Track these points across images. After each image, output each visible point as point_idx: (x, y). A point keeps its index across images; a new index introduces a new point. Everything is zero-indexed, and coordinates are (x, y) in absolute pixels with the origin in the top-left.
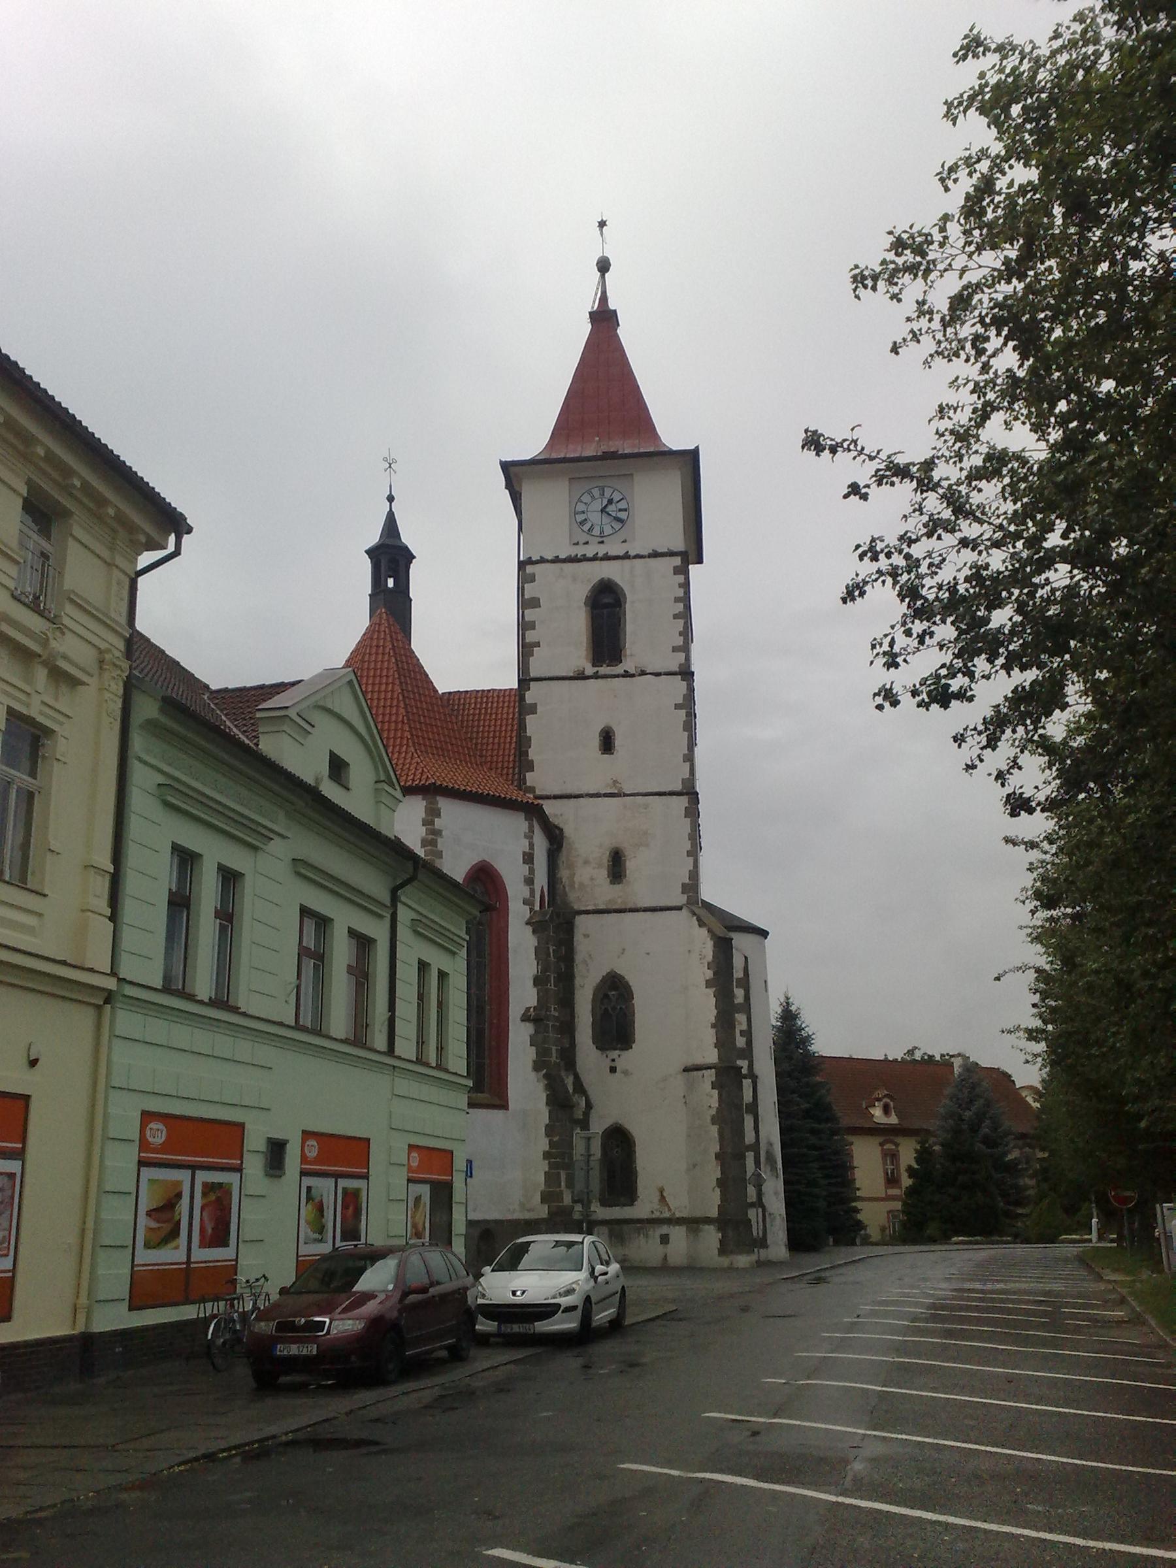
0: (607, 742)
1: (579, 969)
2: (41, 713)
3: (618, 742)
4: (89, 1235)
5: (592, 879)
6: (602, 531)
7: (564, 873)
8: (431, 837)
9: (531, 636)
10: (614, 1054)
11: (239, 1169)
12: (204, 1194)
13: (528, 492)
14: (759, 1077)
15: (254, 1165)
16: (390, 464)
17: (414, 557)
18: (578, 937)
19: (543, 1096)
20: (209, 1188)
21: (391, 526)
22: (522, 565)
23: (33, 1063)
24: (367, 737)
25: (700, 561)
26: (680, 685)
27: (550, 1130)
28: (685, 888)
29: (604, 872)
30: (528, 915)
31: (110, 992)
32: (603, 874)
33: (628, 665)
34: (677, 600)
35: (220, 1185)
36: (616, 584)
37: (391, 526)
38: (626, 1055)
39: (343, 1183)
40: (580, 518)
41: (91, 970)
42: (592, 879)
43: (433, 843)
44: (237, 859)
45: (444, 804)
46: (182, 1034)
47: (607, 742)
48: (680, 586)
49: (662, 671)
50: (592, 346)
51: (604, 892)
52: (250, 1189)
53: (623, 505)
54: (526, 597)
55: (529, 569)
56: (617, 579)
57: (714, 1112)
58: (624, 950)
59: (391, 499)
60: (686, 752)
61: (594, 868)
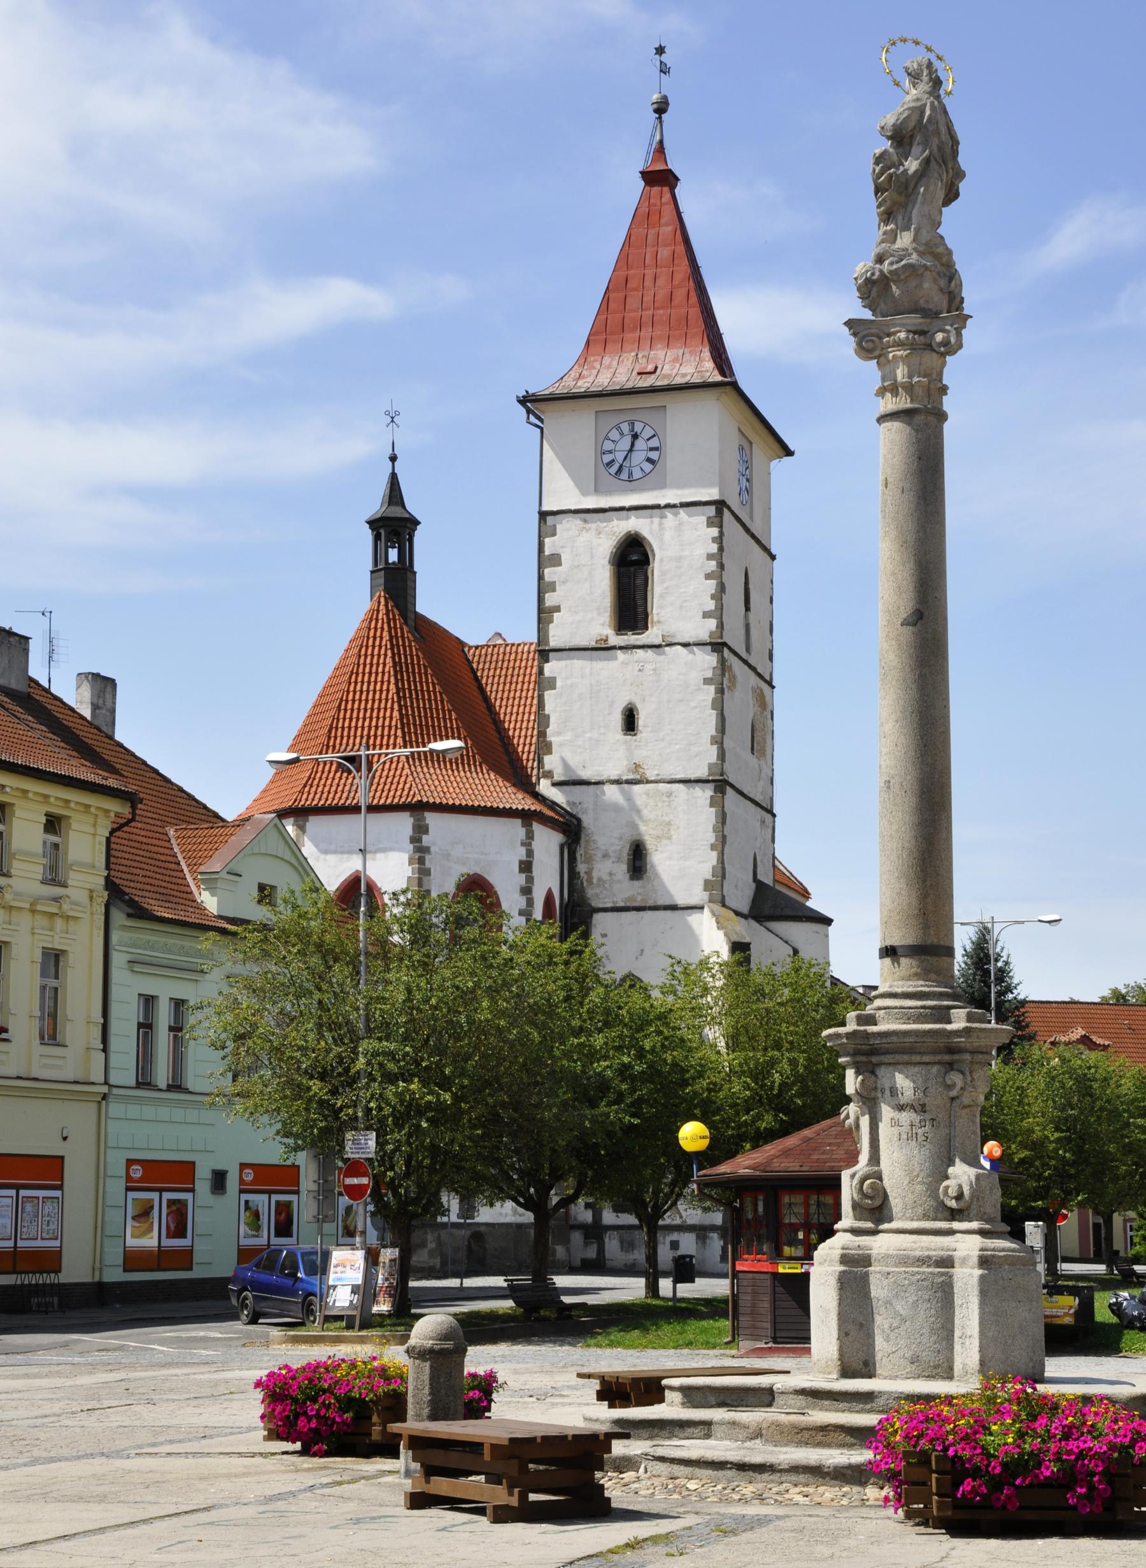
0: (630, 722)
2: (60, 943)
3: (641, 721)
4: (99, 1229)
5: (611, 874)
6: (630, 474)
7: (581, 868)
11: (192, 1190)
12: (168, 1207)
15: (203, 1185)
16: (392, 418)
17: (418, 523)
20: (171, 1202)
21: (395, 494)
22: (543, 515)
23: (65, 1139)
24: (296, 863)
29: (624, 867)
31: (105, 1094)
32: (622, 869)
33: (652, 635)
34: (710, 557)
35: (179, 1201)
37: (395, 494)
39: (275, 1198)
40: (607, 458)
41: (93, 1083)
42: (611, 874)
44: (181, 990)
45: (431, 818)
46: (149, 1112)
47: (630, 722)
49: (691, 641)
50: (644, 217)
51: (624, 889)
52: (199, 1202)
53: (654, 443)
54: (547, 553)
58: (642, 950)
59: (393, 459)
61: (613, 862)
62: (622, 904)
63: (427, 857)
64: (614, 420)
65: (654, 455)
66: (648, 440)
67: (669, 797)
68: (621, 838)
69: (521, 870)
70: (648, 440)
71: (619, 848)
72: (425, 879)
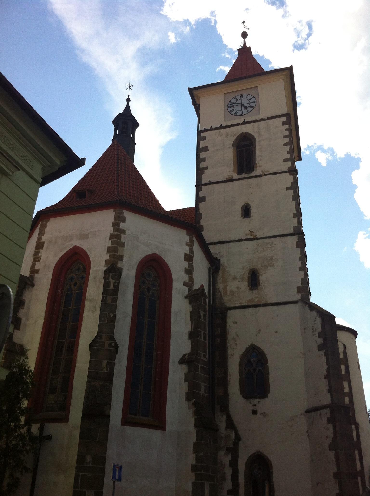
1: (230, 343)
7: (220, 286)
8: (116, 233)
9: (203, 165)
10: (256, 401)
13: (203, 103)
14: (360, 424)
17: (139, 125)
18: (230, 323)
19: (192, 420)
22: (199, 133)
25: (300, 159)
26: (290, 178)
27: (197, 447)
28: (299, 290)
29: (246, 284)
30: (187, 292)
32: (244, 285)
33: (257, 172)
36: (250, 134)
38: (263, 401)
40: (230, 109)
42: (238, 288)
43: (119, 237)
45: (127, 215)
48: (286, 130)
53: (253, 100)
55: (203, 134)
56: (251, 132)
57: (330, 441)
58: (260, 330)
60: (295, 212)
61: (239, 282)
62: (245, 304)
63: (123, 236)
64: (233, 95)
65: (253, 104)
66: (250, 100)
67: (271, 245)
68: (243, 269)
69: (186, 259)
70: (250, 100)
71: (242, 273)
72: (120, 249)
